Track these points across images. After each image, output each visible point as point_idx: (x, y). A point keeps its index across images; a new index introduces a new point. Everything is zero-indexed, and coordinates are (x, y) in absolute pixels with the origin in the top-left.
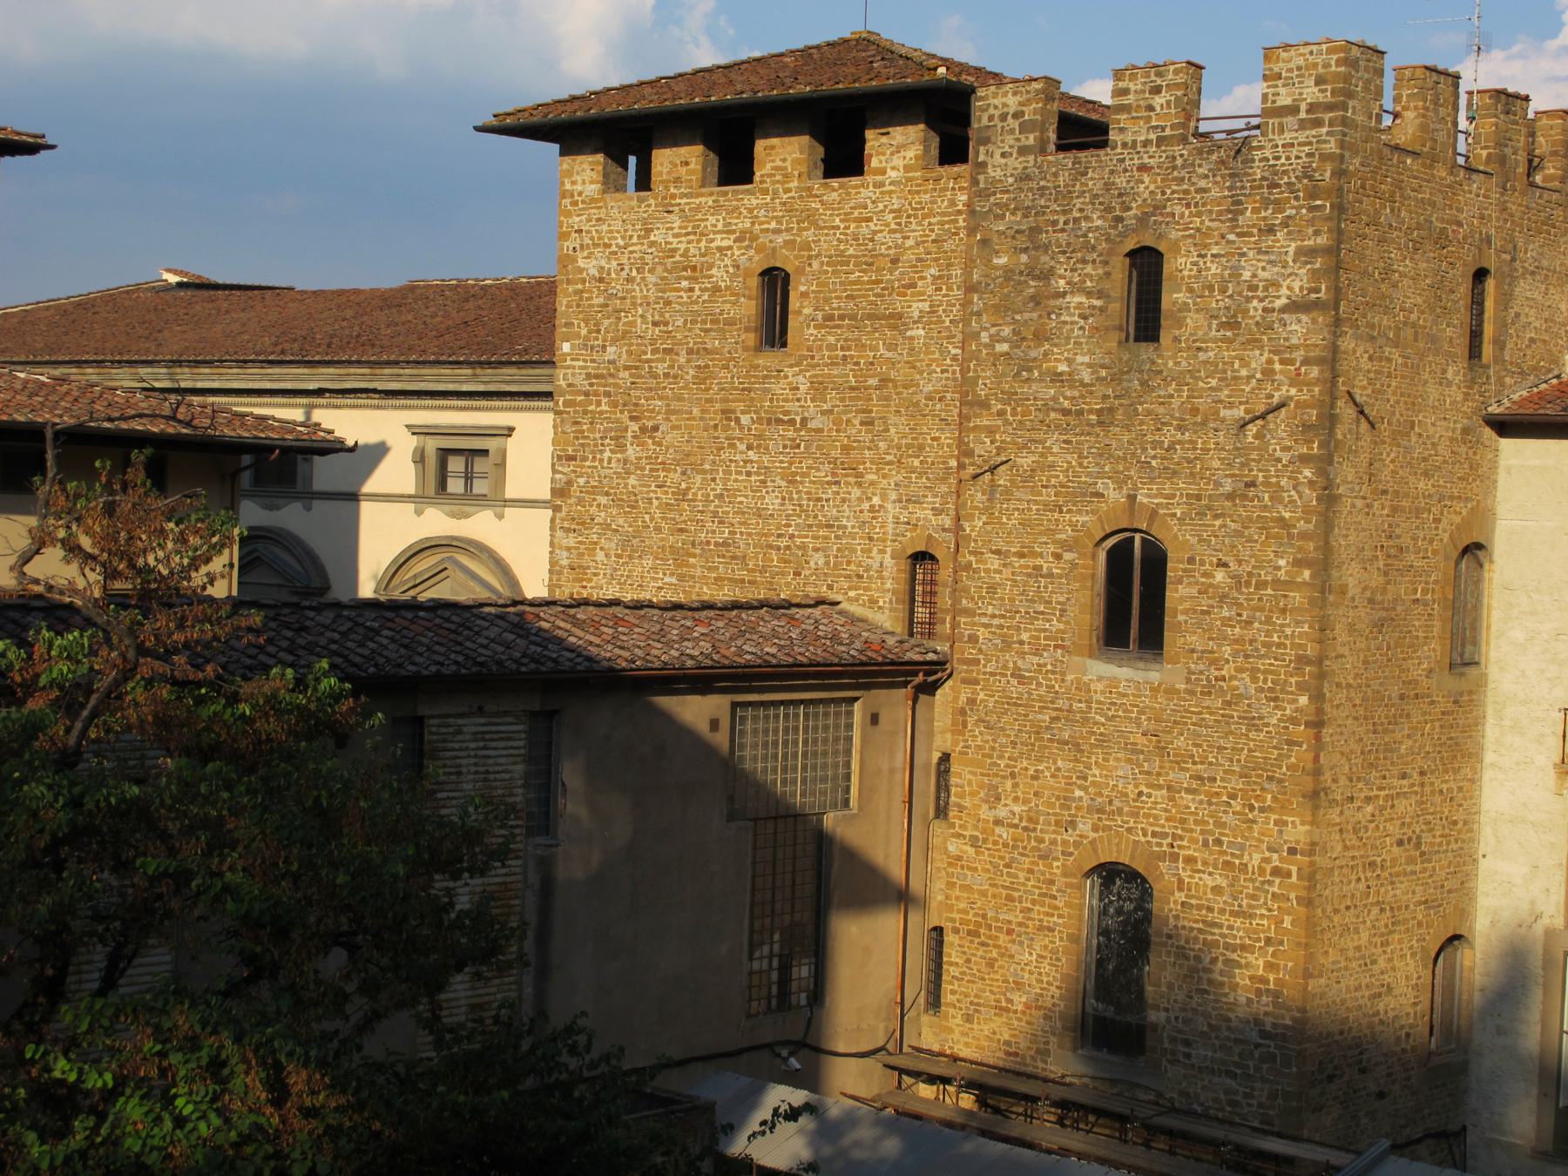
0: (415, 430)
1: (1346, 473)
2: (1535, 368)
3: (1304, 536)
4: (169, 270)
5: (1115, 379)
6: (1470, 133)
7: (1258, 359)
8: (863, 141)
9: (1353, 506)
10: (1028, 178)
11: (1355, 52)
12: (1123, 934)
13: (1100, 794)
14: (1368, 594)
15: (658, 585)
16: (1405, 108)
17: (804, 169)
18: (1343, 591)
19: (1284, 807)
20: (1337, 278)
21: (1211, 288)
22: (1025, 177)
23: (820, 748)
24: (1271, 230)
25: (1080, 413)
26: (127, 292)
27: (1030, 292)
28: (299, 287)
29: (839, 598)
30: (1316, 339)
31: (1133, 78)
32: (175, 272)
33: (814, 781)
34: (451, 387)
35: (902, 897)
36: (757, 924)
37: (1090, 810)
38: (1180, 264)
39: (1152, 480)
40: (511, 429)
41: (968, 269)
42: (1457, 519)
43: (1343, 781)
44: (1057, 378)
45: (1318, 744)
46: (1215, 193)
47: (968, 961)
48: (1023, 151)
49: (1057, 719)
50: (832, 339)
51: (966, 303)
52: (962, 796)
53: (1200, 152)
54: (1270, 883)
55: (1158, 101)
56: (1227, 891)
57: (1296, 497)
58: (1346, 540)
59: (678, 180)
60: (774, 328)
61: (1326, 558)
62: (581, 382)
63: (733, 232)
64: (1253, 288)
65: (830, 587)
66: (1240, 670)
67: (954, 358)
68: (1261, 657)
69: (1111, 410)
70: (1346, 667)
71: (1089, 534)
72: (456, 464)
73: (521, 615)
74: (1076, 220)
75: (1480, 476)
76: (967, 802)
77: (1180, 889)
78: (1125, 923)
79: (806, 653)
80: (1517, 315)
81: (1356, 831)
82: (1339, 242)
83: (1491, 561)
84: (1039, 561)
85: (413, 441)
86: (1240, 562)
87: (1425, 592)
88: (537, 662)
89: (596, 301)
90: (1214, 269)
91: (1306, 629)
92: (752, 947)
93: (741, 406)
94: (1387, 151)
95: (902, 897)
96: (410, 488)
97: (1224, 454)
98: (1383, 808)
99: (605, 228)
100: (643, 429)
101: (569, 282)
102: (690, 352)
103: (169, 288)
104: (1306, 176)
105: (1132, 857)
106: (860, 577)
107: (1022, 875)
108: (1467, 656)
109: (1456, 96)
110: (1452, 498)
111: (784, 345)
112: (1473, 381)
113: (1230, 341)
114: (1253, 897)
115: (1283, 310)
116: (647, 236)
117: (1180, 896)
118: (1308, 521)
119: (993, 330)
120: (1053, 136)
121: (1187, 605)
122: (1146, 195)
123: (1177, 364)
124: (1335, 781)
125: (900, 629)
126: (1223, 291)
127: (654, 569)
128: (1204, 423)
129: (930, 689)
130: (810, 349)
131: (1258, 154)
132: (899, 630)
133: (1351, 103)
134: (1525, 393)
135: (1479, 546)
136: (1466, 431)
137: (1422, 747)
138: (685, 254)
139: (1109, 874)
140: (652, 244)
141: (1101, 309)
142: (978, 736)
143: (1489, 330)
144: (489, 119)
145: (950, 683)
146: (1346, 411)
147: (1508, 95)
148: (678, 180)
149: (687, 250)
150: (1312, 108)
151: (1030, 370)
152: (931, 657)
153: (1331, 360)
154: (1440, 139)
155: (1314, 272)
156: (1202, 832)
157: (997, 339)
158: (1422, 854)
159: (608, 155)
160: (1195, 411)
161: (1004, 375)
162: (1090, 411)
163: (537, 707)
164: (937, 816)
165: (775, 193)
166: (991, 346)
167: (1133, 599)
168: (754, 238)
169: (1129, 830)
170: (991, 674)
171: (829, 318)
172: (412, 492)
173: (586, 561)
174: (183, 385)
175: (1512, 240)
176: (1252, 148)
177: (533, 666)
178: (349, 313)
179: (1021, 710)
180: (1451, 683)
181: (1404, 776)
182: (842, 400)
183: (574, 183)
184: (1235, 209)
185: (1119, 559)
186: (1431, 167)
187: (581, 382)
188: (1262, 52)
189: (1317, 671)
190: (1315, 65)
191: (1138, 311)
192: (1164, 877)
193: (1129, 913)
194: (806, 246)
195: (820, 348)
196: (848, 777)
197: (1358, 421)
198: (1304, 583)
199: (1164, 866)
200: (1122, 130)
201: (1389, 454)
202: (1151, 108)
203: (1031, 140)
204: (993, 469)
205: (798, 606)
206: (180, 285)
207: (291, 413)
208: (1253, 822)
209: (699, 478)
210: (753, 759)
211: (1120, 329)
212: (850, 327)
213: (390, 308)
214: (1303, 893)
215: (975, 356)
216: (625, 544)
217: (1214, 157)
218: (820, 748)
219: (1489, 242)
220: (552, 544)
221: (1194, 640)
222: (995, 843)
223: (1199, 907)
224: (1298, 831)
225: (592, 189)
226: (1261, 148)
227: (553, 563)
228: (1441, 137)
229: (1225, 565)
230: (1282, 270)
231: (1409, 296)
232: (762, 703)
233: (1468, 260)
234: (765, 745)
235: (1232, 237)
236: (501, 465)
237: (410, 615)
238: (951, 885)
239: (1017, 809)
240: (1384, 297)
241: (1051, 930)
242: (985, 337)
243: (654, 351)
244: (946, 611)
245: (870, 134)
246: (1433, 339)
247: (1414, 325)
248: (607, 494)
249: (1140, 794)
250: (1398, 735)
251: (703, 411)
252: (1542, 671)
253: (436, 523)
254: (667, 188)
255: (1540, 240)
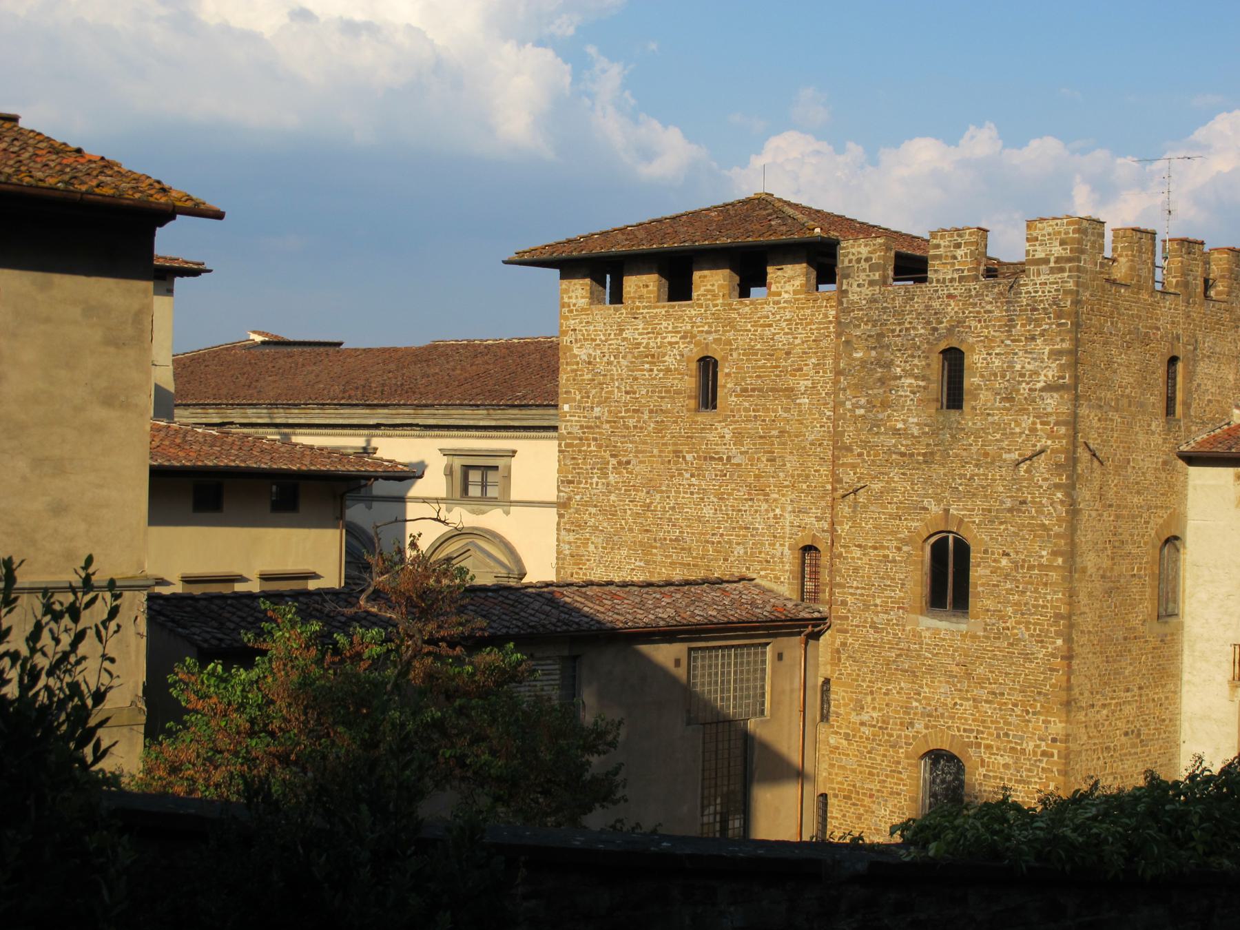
0: (446, 453)
1: (1084, 494)
2: (1212, 419)
3: (1057, 536)
4: (255, 332)
5: (935, 433)
6: (1166, 270)
7: (1027, 421)
8: (765, 274)
9: (1090, 515)
10: (875, 301)
11: (1085, 224)
12: (946, 796)
13: (930, 705)
14: (1101, 572)
15: (629, 569)
16: (1120, 256)
17: (726, 292)
18: (1084, 570)
19: (1047, 711)
20: (1076, 369)
21: (995, 375)
22: (873, 300)
23: (745, 676)
24: (1033, 338)
25: (912, 455)
26: (227, 349)
27: (879, 375)
28: (350, 343)
29: (754, 576)
30: (1063, 409)
31: (943, 237)
32: (259, 333)
33: (741, 698)
34: (471, 423)
35: (800, 775)
36: (706, 792)
37: (923, 715)
38: (975, 359)
39: (959, 500)
40: (515, 452)
41: (837, 359)
42: (1161, 521)
43: (1087, 694)
44: (896, 432)
45: (1070, 671)
46: (997, 313)
47: (844, 816)
48: (872, 283)
49: (900, 655)
50: (746, 404)
51: (836, 383)
52: (838, 706)
53: (987, 286)
54: (1040, 761)
55: (959, 253)
56: (1013, 767)
57: (1052, 512)
58: (1085, 538)
59: (641, 297)
60: (708, 397)
61: (1072, 550)
62: (576, 430)
63: (679, 332)
64: (1022, 375)
65: (748, 569)
66: (1018, 623)
67: (828, 418)
68: (1032, 614)
69: (932, 454)
70: (1087, 620)
71: (919, 534)
72: (475, 476)
73: (551, 593)
74: (907, 329)
75: (1175, 491)
76: (842, 711)
77: (983, 766)
78: (947, 789)
79: (735, 615)
80: (1199, 385)
81: (1096, 726)
82: (1077, 346)
83: (1184, 547)
84: (887, 552)
85: (444, 461)
86: (1017, 553)
87: (1140, 569)
88: (566, 624)
89: (586, 377)
90: (997, 363)
91: (1060, 595)
92: (703, 808)
93: (686, 448)
94: (1107, 286)
95: (800, 775)
96: (443, 493)
97: (1005, 483)
98: (1113, 712)
99: (592, 328)
100: (620, 463)
101: (567, 364)
102: (651, 412)
103: (256, 345)
104: (1054, 303)
105: (951, 746)
106: (768, 562)
107: (879, 758)
108: (1169, 610)
109: (1154, 245)
110: (1156, 507)
111: (715, 407)
112: (1169, 430)
113: (1008, 410)
114: (1029, 770)
115: (1042, 390)
116: (620, 334)
117: (983, 771)
118: (1060, 527)
119: (854, 400)
120: (891, 273)
121: (984, 581)
122: (952, 314)
123: (974, 424)
124: (1081, 694)
125: (795, 596)
126: (1003, 377)
127: (629, 556)
128: (992, 463)
129: (816, 636)
130: (732, 411)
131: (1024, 289)
132: (794, 597)
133: (1083, 257)
134: (1205, 436)
135: (1176, 538)
136: (1165, 463)
137: (1140, 671)
138: (647, 347)
139: (936, 757)
140: (624, 339)
141: (925, 388)
142: (848, 667)
143: (1179, 396)
144: (511, 255)
145: (829, 632)
146: (1083, 455)
147: (1190, 242)
148: (641, 297)
149: (648, 344)
150: (1058, 260)
151: (878, 426)
152: (816, 615)
153: (1073, 422)
154: (1143, 275)
155: (1061, 365)
156: (996, 729)
157: (856, 406)
158: (1142, 741)
159: (593, 279)
160: (986, 455)
161: (862, 430)
162: (919, 454)
163: (566, 653)
164: (822, 720)
165: (707, 306)
166: (852, 411)
167: (948, 576)
168: (693, 337)
169: (949, 728)
170: (857, 626)
171: (745, 390)
172: (444, 495)
173: (582, 551)
174: (278, 421)
175: (1194, 336)
176: (1020, 285)
177: (565, 628)
178: (392, 366)
179: (877, 650)
180: (1158, 628)
181: (1128, 690)
182: (754, 444)
183: (570, 298)
184: (1010, 323)
185: (939, 550)
186: (1138, 293)
187: (576, 430)
188: (1025, 224)
189: (1068, 623)
190: (1059, 233)
191: (948, 389)
192: (971, 758)
193: (950, 782)
194: (729, 342)
195: (739, 410)
196: (763, 695)
197: (1092, 461)
198: (1059, 566)
199: (971, 751)
200: (936, 271)
201: (1113, 481)
202: (955, 257)
203: (877, 276)
204: (855, 492)
205: (728, 582)
206: (263, 343)
207: (354, 441)
208: (1029, 721)
209: (658, 496)
210: (704, 686)
211: (937, 400)
212: (758, 396)
213: (420, 362)
214: (1061, 767)
215: (843, 417)
216: (608, 539)
217: (996, 290)
218: (745, 676)
219: (1178, 339)
220: (558, 540)
221: (989, 603)
222: (861, 737)
223: (995, 778)
224: (1057, 727)
225: (583, 302)
226: (1026, 285)
227: (559, 552)
228: (1144, 273)
229: (1008, 555)
230: (1040, 363)
231: (1125, 378)
232: (707, 648)
233: (1165, 351)
234: (710, 675)
235: (1008, 342)
236: (508, 477)
237: (483, 595)
238: (832, 766)
239: (875, 715)
240: (1107, 379)
241: (899, 794)
242: (848, 405)
243: (627, 411)
244: (826, 585)
245: (770, 269)
246: (1142, 405)
247: (1128, 397)
248: (596, 506)
249: (955, 704)
250: (1123, 664)
251: (660, 451)
252: (1220, 620)
253: (461, 516)
254: (634, 302)
255: (1214, 334)
